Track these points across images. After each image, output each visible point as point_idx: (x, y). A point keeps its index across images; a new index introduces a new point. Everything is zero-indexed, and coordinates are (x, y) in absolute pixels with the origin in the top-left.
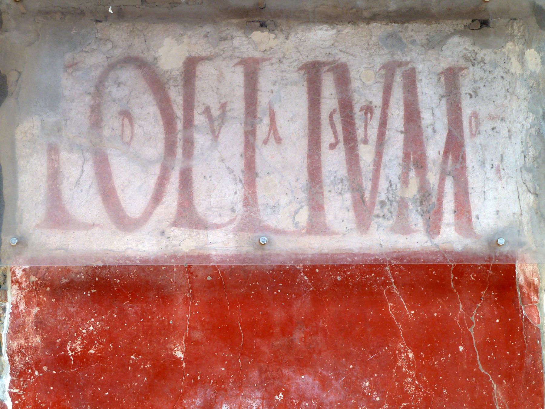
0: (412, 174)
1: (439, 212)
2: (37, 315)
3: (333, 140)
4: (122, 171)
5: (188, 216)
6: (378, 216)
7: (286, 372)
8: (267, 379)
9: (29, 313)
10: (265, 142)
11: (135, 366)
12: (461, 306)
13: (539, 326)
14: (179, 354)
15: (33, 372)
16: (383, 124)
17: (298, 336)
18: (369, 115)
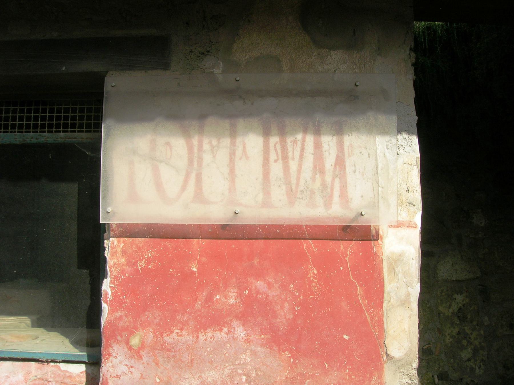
0: (318, 176)
1: (331, 196)
2: (123, 248)
3: (276, 158)
4: (165, 172)
5: (199, 196)
6: (299, 198)
7: (249, 279)
8: (239, 283)
9: (119, 246)
10: (240, 159)
11: (172, 274)
12: (342, 246)
13: (382, 257)
14: (194, 269)
15: (121, 276)
16: (303, 149)
17: (256, 261)
18: (295, 145)
